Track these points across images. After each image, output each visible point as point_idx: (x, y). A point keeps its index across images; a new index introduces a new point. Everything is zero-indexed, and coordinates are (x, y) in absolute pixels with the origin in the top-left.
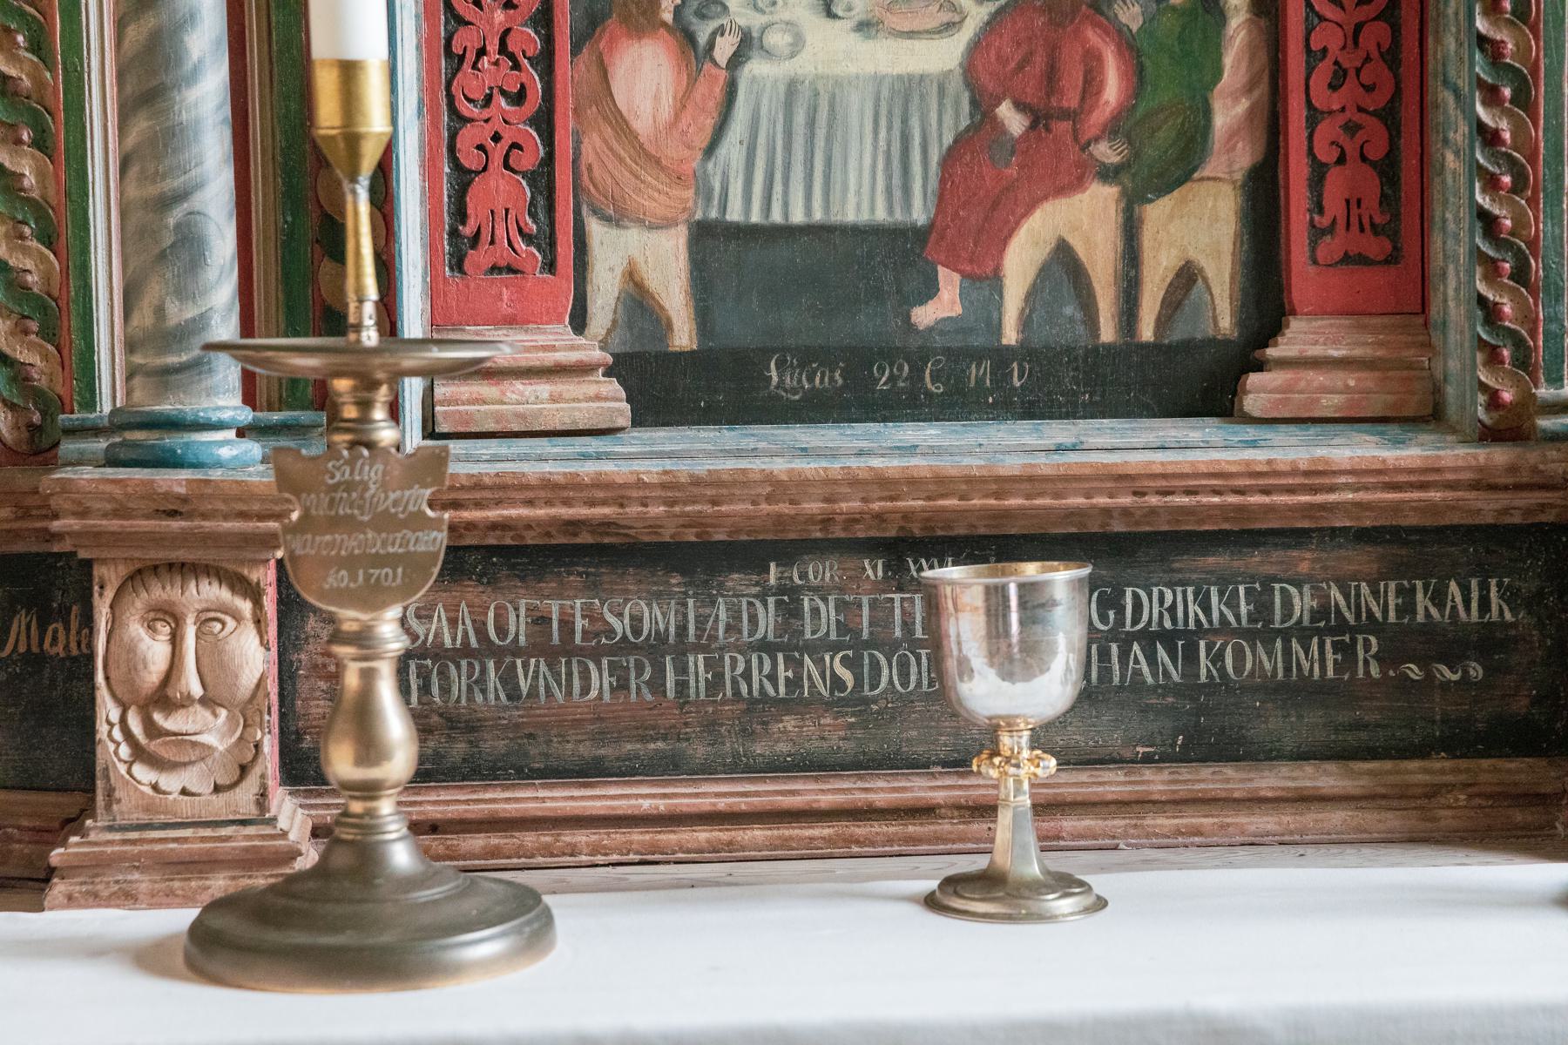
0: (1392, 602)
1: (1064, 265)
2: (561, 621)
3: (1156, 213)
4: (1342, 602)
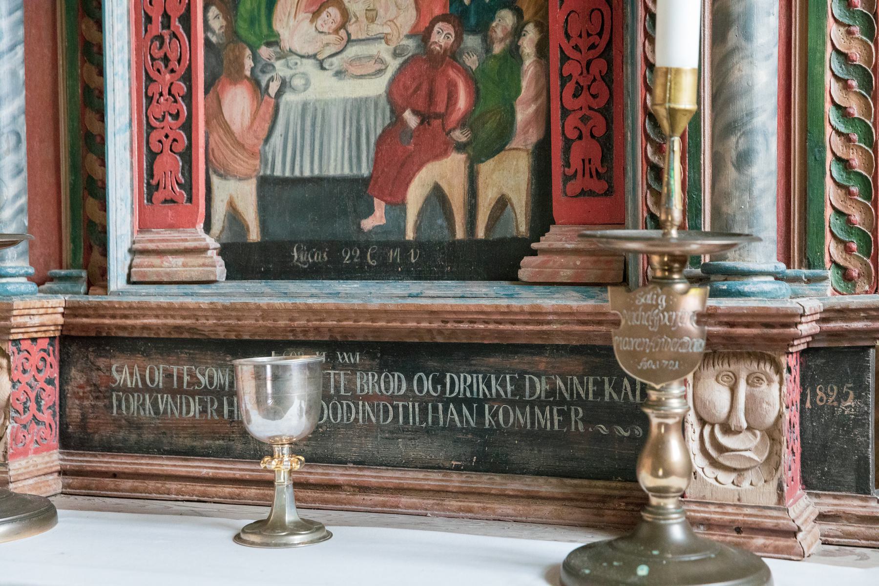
0: (509, 388)
1: (438, 197)
2: (178, 377)
3: (485, 168)
4: (563, 388)
